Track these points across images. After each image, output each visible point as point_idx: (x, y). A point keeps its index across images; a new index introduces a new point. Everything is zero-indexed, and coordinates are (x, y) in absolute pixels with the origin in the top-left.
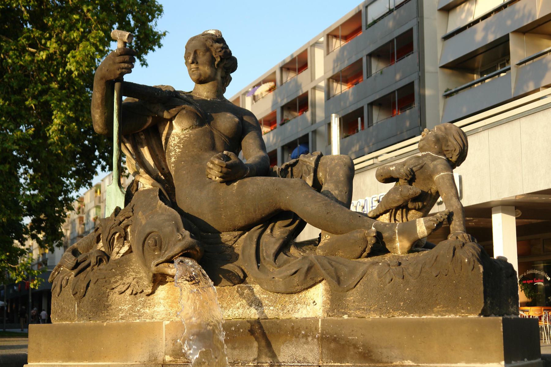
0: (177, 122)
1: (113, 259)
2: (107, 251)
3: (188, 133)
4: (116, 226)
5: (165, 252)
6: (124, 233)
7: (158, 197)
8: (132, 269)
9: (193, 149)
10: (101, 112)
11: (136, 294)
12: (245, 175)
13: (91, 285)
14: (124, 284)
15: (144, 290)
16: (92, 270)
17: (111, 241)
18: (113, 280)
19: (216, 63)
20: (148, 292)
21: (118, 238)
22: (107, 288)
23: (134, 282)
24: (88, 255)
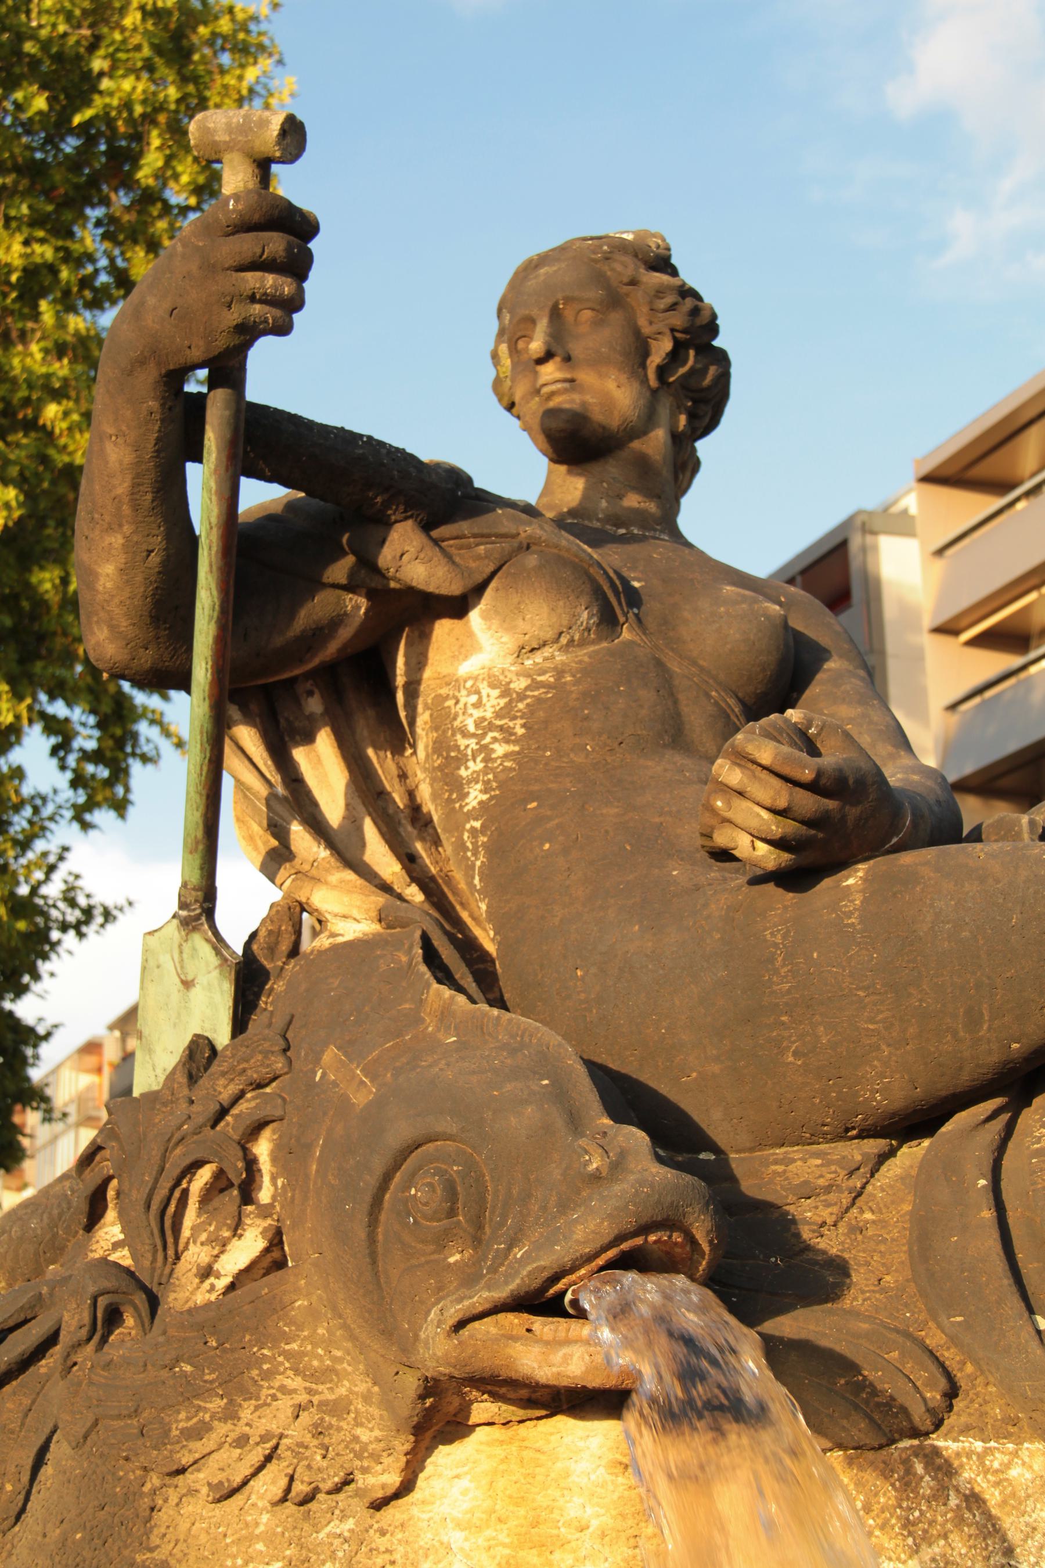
0: (496, 612)
1: (178, 1306)
2: (147, 1263)
3: (549, 664)
4: (198, 1130)
5: (509, 1248)
6: (240, 1164)
7: (423, 968)
8: (288, 1355)
9: (577, 740)
10: (128, 546)
11: (308, 1499)
12: (895, 840)
13: (59, 1450)
14: (242, 1441)
15: (358, 1476)
16: (69, 1368)
17: (172, 1208)
18: (182, 1421)
19: (656, 359)
20: (383, 1486)
21: (207, 1196)
22: (145, 1469)
23: (297, 1433)
24: (45, 1290)
